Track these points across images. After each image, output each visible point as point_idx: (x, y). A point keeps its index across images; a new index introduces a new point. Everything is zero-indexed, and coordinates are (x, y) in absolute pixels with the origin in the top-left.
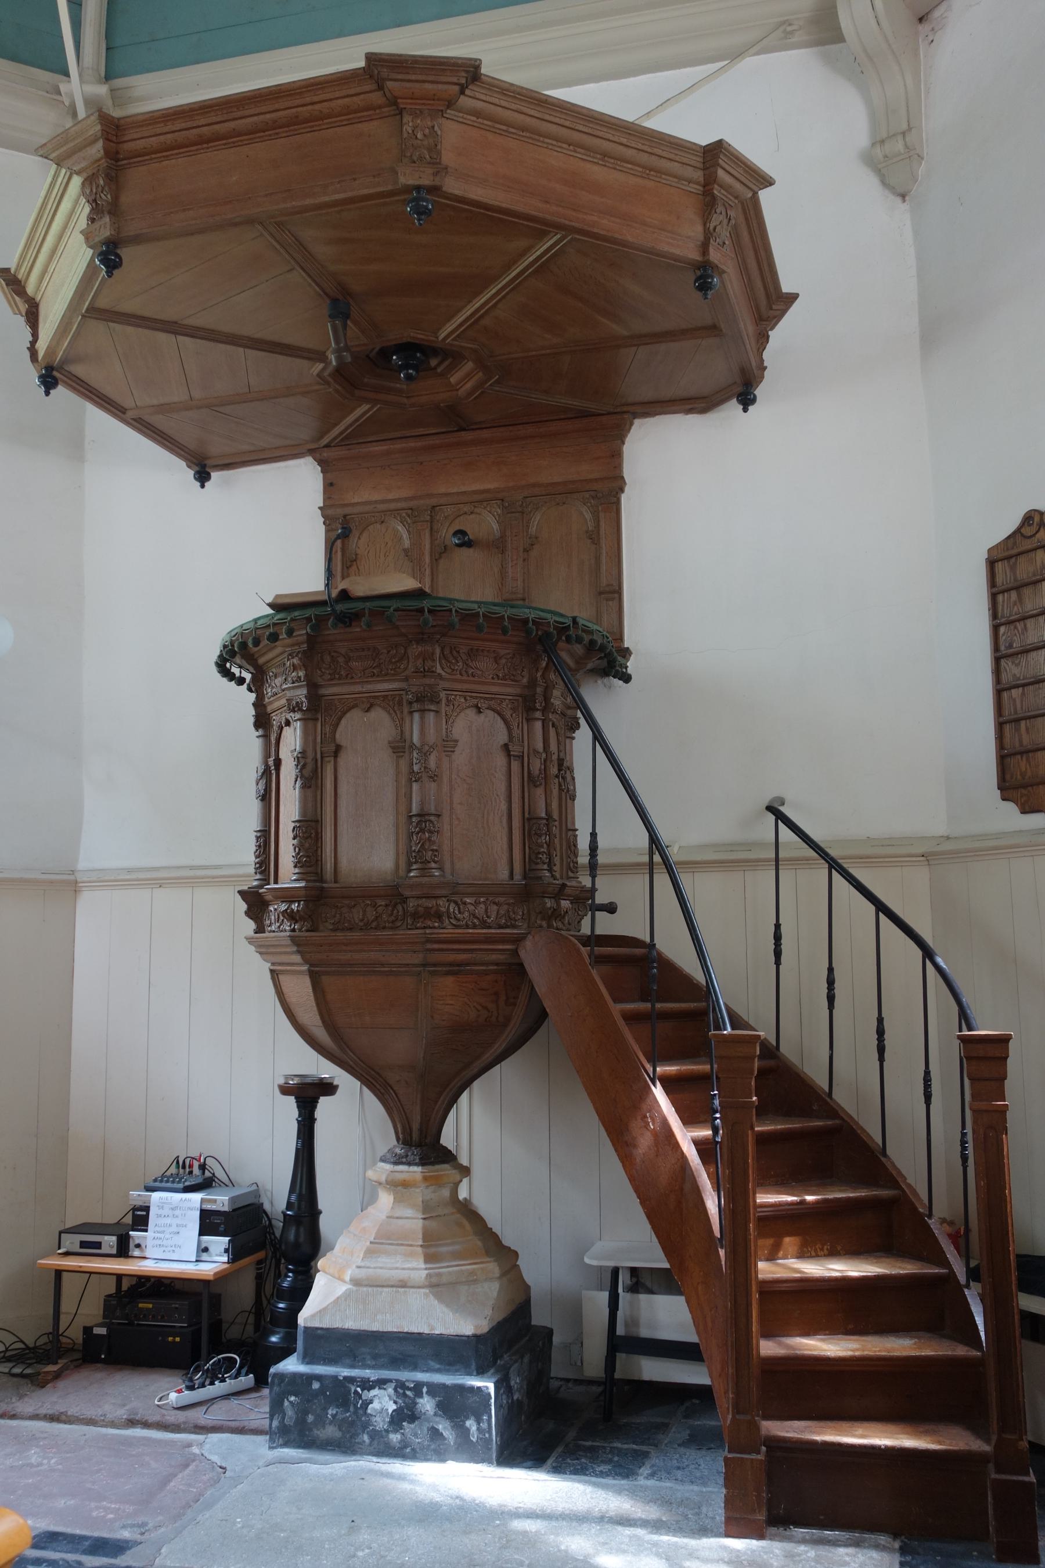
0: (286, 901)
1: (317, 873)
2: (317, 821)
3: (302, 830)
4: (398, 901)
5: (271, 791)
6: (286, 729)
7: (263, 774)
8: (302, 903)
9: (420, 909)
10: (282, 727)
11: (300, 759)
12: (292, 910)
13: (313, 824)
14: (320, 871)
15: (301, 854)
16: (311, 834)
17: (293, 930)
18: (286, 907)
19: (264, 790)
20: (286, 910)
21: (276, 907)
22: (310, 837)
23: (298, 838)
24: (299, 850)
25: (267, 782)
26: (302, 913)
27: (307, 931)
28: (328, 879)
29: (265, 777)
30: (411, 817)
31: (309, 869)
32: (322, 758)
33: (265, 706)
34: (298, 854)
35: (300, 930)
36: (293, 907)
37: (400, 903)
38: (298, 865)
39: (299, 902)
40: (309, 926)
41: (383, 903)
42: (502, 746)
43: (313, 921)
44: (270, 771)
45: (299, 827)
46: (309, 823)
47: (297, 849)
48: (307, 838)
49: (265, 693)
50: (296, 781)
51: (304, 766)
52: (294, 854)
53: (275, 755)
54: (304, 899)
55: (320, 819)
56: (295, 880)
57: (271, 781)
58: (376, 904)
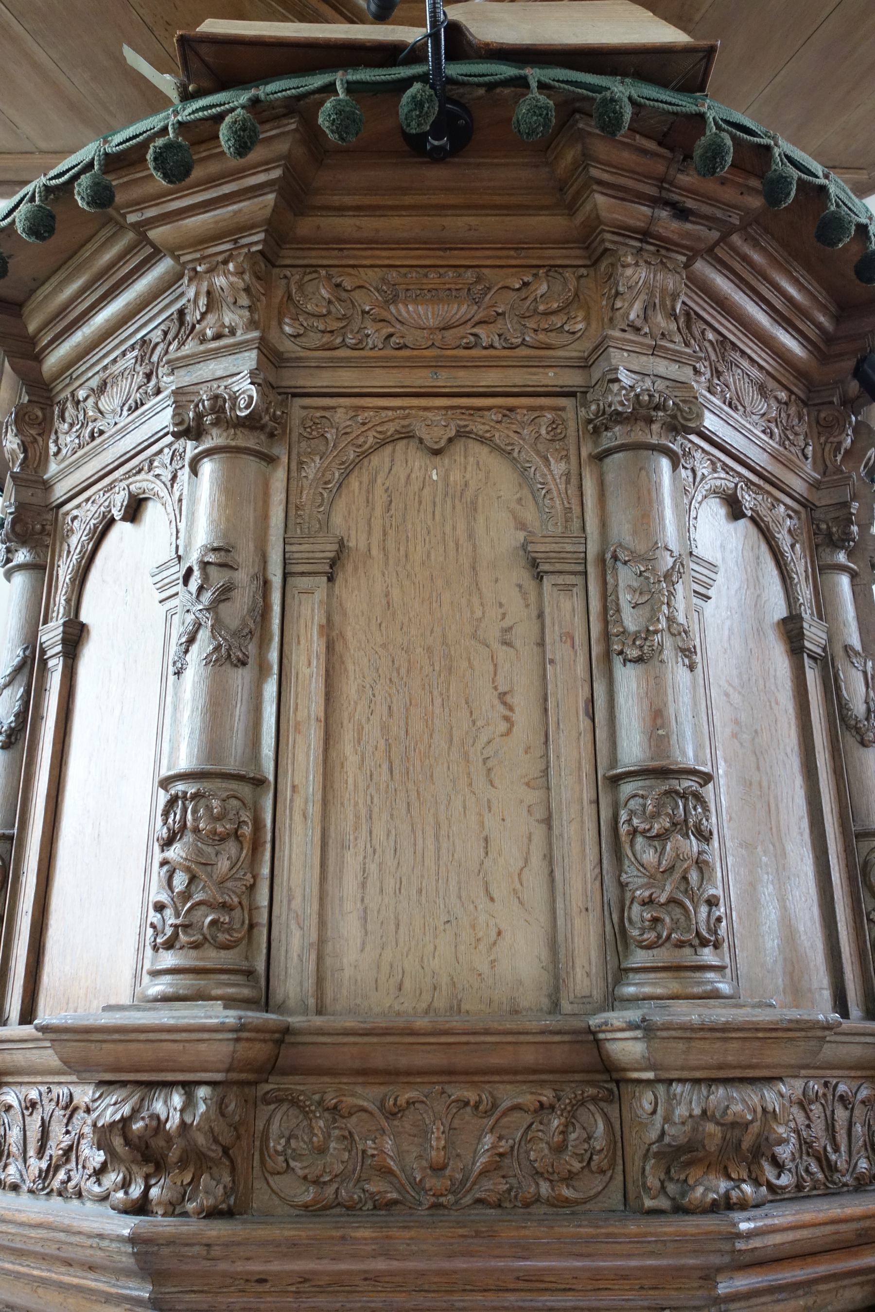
0: (123, 1084)
1: (249, 973)
2: (259, 782)
3: (209, 809)
4: (591, 1091)
5: (38, 718)
6: (121, 530)
7: (18, 670)
8: (202, 1092)
9: (711, 1127)
10: (112, 521)
11: (212, 570)
12: (159, 1124)
13: (245, 790)
14: (261, 967)
15: (198, 897)
16: (240, 824)
17: (141, 1207)
18: (126, 1110)
19: (17, 715)
20: (125, 1122)
21: (33, 1094)
22: (236, 835)
23: (189, 837)
24: (193, 879)
25: (28, 692)
26: (201, 1140)
27: (212, 1214)
28: (291, 1003)
29: (22, 679)
30: (615, 781)
31: (223, 953)
32: (285, 576)
33: (47, 487)
34: (186, 895)
35: (173, 1208)
36: (159, 1107)
37: (594, 1099)
38: (183, 938)
39: (188, 1087)
40: (220, 1190)
41: (527, 1099)
42: (778, 623)
43: (233, 1170)
44: (44, 662)
45: (196, 796)
46: (234, 785)
47: (180, 881)
48: (223, 839)
49: (53, 448)
50: (191, 640)
51: (225, 594)
52: (164, 897)
53: (67, 613)
54: (219, 1077)
55: (271, 778)
56: (166, 999)
57: (42, 689)
58: (495, 1106)
